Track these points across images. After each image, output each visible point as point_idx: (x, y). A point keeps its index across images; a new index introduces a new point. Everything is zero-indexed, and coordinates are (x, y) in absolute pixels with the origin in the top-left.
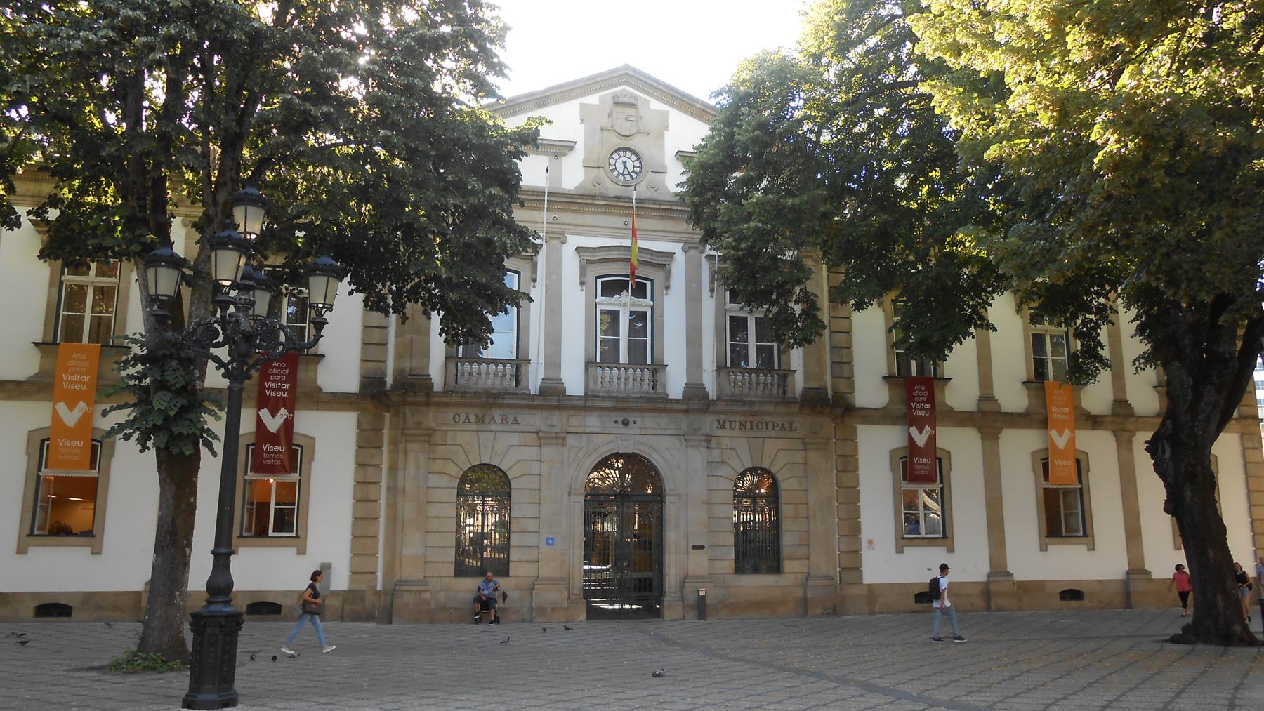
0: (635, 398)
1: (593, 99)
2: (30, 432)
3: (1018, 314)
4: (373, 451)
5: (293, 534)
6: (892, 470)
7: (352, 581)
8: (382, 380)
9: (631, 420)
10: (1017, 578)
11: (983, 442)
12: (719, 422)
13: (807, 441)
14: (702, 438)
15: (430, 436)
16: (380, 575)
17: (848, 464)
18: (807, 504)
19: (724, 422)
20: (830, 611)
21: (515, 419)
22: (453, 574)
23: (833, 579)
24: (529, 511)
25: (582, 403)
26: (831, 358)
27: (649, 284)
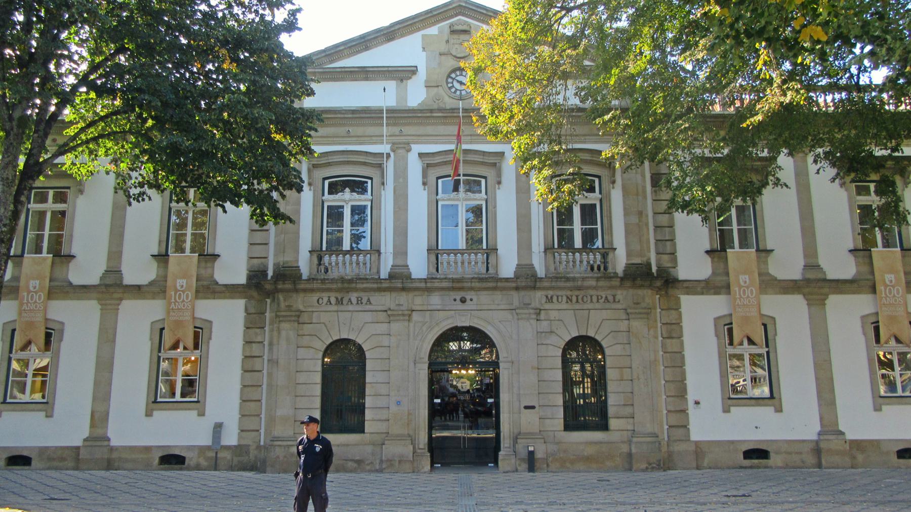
0: (469, 279)
1: (433, 30)
2: (4, 324)
3: (841, 187)
4: (258, 331)
5: (196, 400)
6: (717, 335)
7: (240, 437)
8: (264, 273)
9: (468, 298)
10: (850, 436)
11: (809, 308)
12: (547, 297)
13: (629, 311)
14: (532, 311)
15: (299, 316)
16: (262, 431)
17: (674, 331)
18: (631, 368)
19: (552, 297)
20: (655, 465)
21: (369, 300)
22: (563, 429)
23: (657, 437)
24: (381, 377)
25: (423, 285)
26: (655, 236)
27: (483, 181)
